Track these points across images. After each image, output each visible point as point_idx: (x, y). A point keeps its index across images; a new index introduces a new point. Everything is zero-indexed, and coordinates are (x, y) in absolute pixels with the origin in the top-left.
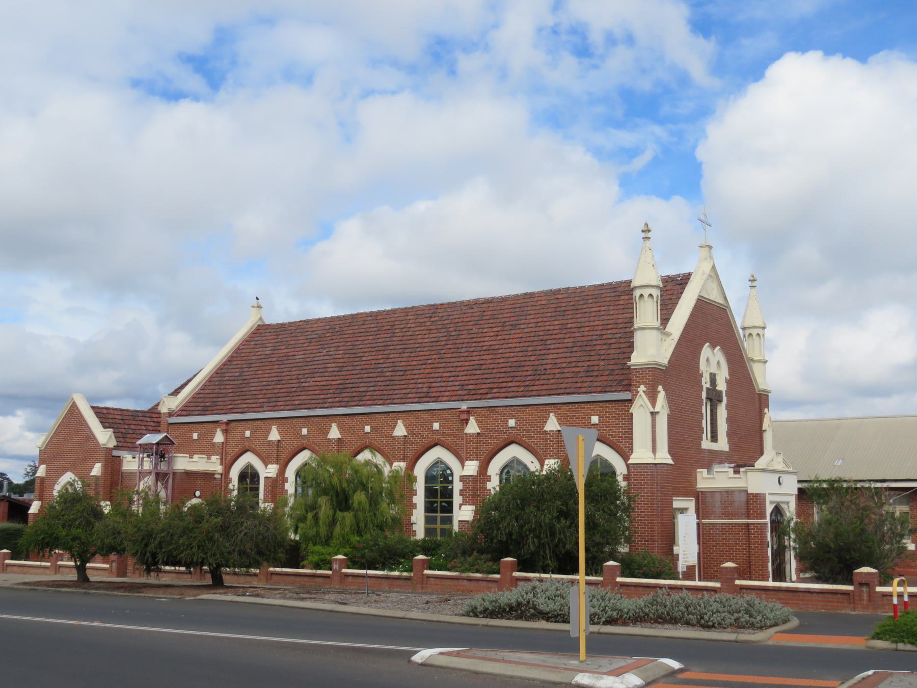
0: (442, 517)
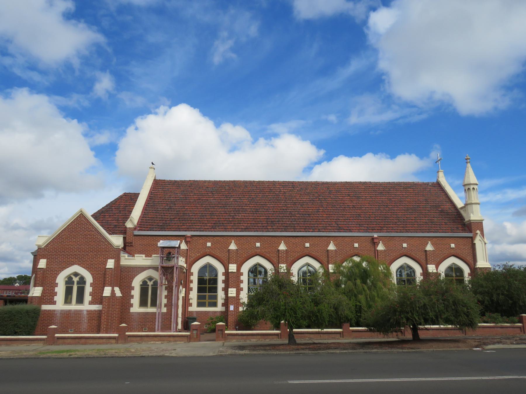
0: (209, 295)
